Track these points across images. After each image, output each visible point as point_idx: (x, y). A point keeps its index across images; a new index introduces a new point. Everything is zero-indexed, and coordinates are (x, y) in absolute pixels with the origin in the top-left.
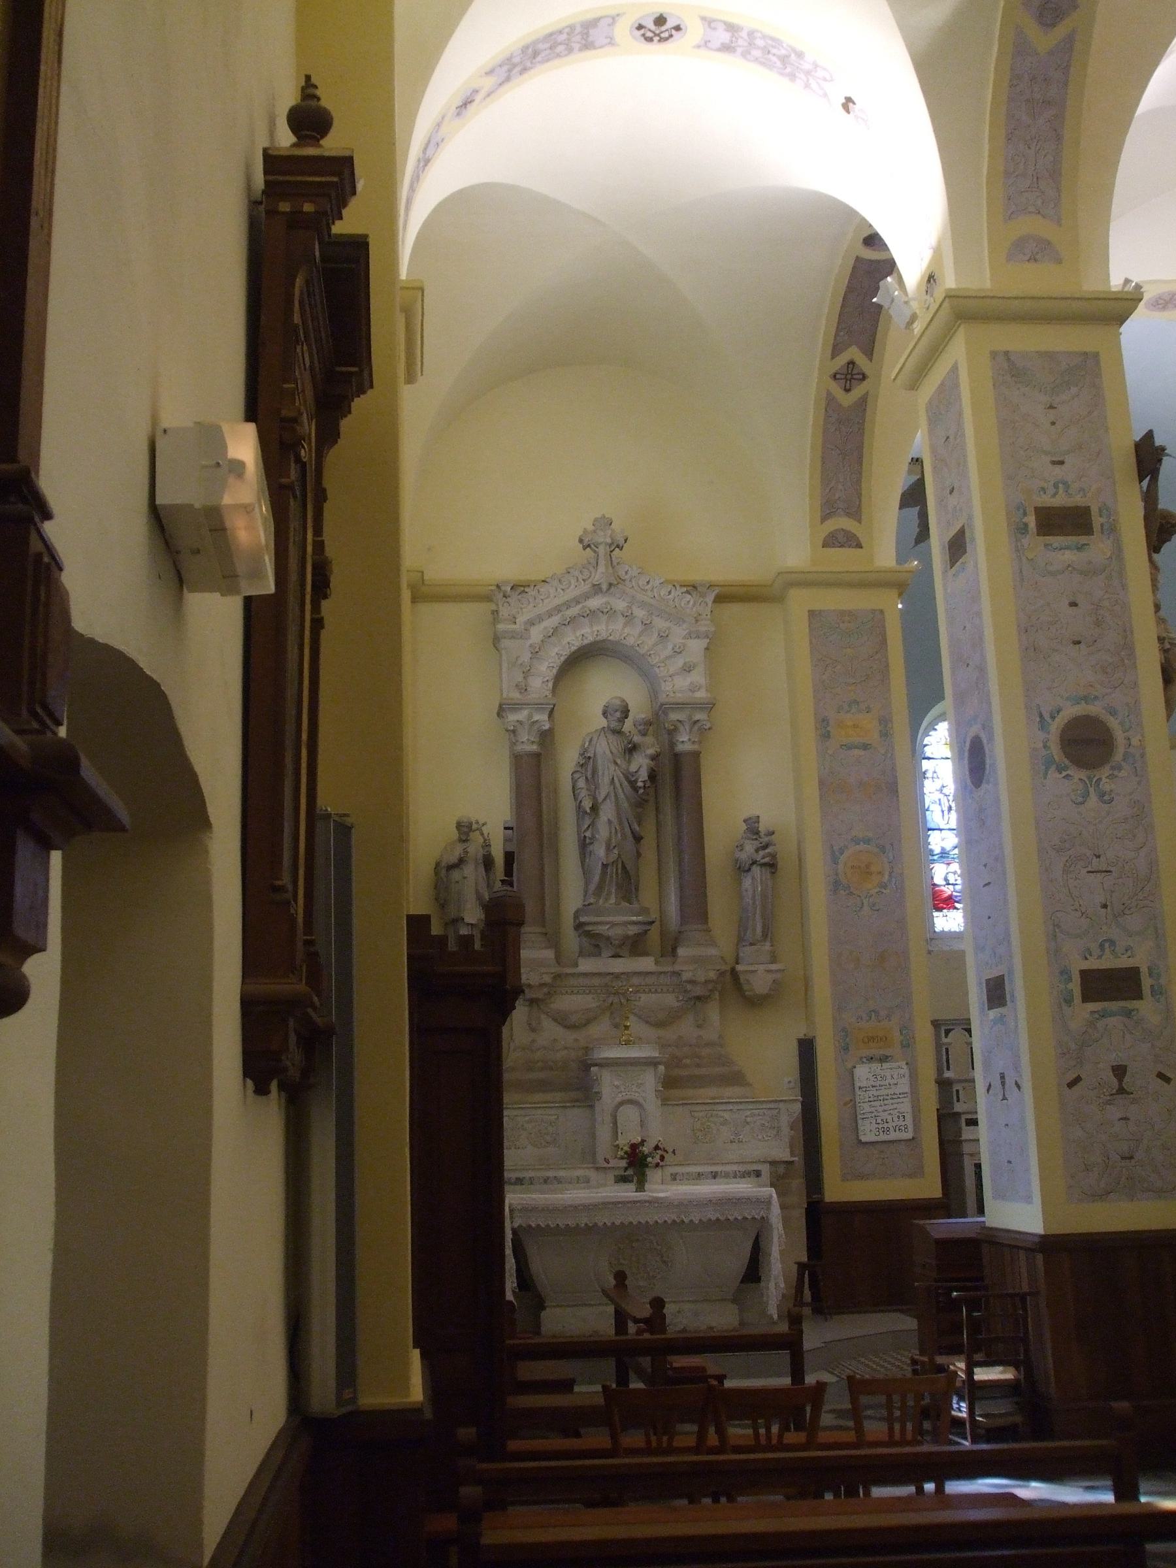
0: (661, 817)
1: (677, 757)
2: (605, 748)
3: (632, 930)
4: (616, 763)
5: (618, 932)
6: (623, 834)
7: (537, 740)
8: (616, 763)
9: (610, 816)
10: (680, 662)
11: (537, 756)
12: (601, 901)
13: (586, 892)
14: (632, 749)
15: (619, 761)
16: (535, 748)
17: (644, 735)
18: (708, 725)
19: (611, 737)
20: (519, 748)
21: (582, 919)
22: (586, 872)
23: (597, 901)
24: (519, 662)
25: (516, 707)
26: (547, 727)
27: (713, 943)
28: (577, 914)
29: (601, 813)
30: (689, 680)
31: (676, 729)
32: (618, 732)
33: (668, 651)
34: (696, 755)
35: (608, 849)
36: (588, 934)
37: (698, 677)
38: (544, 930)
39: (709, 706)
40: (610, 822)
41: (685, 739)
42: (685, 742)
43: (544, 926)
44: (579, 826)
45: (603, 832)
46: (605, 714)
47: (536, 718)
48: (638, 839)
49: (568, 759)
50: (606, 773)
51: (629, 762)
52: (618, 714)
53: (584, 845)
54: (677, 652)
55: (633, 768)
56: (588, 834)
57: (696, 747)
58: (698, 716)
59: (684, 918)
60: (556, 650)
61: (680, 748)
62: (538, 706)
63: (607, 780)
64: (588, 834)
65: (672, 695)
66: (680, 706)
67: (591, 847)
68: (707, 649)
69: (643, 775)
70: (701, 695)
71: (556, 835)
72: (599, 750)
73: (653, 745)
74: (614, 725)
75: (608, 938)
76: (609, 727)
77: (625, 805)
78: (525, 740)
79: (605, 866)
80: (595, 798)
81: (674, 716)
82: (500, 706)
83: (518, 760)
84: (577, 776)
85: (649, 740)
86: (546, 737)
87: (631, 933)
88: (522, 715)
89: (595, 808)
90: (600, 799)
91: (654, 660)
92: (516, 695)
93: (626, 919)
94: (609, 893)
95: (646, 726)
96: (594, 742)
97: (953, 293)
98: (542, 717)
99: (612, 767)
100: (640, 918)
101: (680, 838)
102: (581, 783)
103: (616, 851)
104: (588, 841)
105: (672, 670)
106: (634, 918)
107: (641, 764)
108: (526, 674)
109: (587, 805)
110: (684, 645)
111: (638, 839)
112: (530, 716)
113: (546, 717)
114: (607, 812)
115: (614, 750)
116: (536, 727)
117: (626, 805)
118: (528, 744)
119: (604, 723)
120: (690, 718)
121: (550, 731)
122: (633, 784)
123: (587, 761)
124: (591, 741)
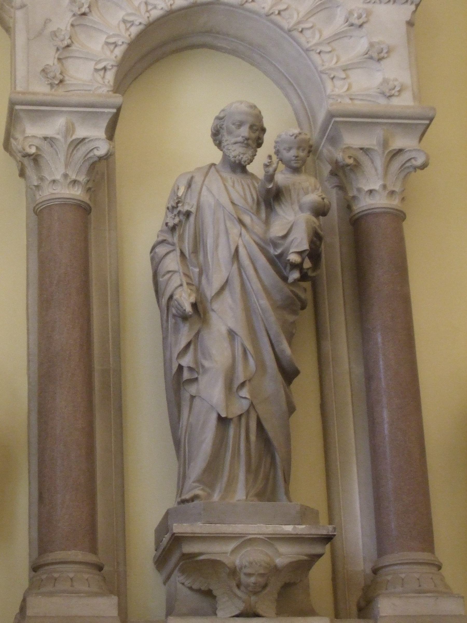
0: (327, 346)
1: (357, 226)
2: (220, 196)
3: (286, 555)
4: (241, 222)
5: (251, 558)
6: (261, 364)
7: (82, 178)
8: (241, 222)
9: (232, 324)
10: (361, 45)
11: (84, 210)
12: (216, 497)
13: (182, 477)
14: (272, 197)
15: (247, 219)
16: (77, 193)
17: (296, 170)
18: (419, 162)
19: (230, 177)
20: (48, 192)
21: (179, 528)
22: (180, 444)
23: (209, 495)
24: (52, 27)
25: (41, 109)
26: (102, 151)
27: (444, 592)
28: (163, 527)
29: (214, 318)
30: (378, 78)
31: (356, 166)
32: (240, 168)
33: (339, 22)
34: (398, 216)
35: (231, 388)
36: (191, 564)
37: (396, 70)
38: (91, 558)
39: (422, 124)
40: (232, 334)
41: (377, 186)
42: (373, 191)
43: (94, 550)
44: (166, 345)
45: (218, 352)
46: (216, 135)
47: (80, 133)
48: (289, 374)
49: (141, 225)
50: (222, 240)
51: (267, 222)
52: (245, 131)
53: (179, 383)
54: (357, 25)
55: (277, 230)
56: (187, 361)
57: (395, 203)
58: (398, 143)
59: (382, 540)
60: (121, 14)
61: (364, 204)
62: (87, 109)
63: (224, 254)
64: (187, 361)
65: (348, 101)
66: (364, 120)
67: (193, 389)
68: (410, 24)
69: (300, 242)
70: (405, 102)
71: (119, 372)
72: (207, 199)
73: (316, 189)
74: (236, 152)
75: (234, 572)
76: (225, 158)
77: (262, 302)
78: (58, 177)
79: (223, 421)
80: (199, 291)
81: (353, 140)
82: (12, 104)
83: (41, 214)
84: (161, 250)
85: (305, 180)
86: (100, 172)
87: (280, 561)
88: (54, 127)
89: (200, 311)
90: (210, 292)
91: (310, 39)
92: (40, 89)
93: (270, 529)
94: (232, 481)
95: (303, 156)
96: (196, 187)
97: (380, 251)
98: (94, 132)
99: (235, 229)
100: (302, 529)
101: (369, 377)
102: (172, 263)
103: (244, 393)
104: (186, 375)
105: (345, 59)
106: (289, 529)
107: (293, 226)
108: (65, 51)
109: (185, 299)
110: (369, 13)
111: (289, 374)
112: (70, 129)
113: (100, 133)
114: (226, 316)
115: (240, 202)
116: (83, 149)
117: (264, 302)
118: (62, 182)
119: (216, 156)
120: (385, 144)
121: (107, 157)
122: (278, 263)
123: (181, 219)
124: (189, 186)
